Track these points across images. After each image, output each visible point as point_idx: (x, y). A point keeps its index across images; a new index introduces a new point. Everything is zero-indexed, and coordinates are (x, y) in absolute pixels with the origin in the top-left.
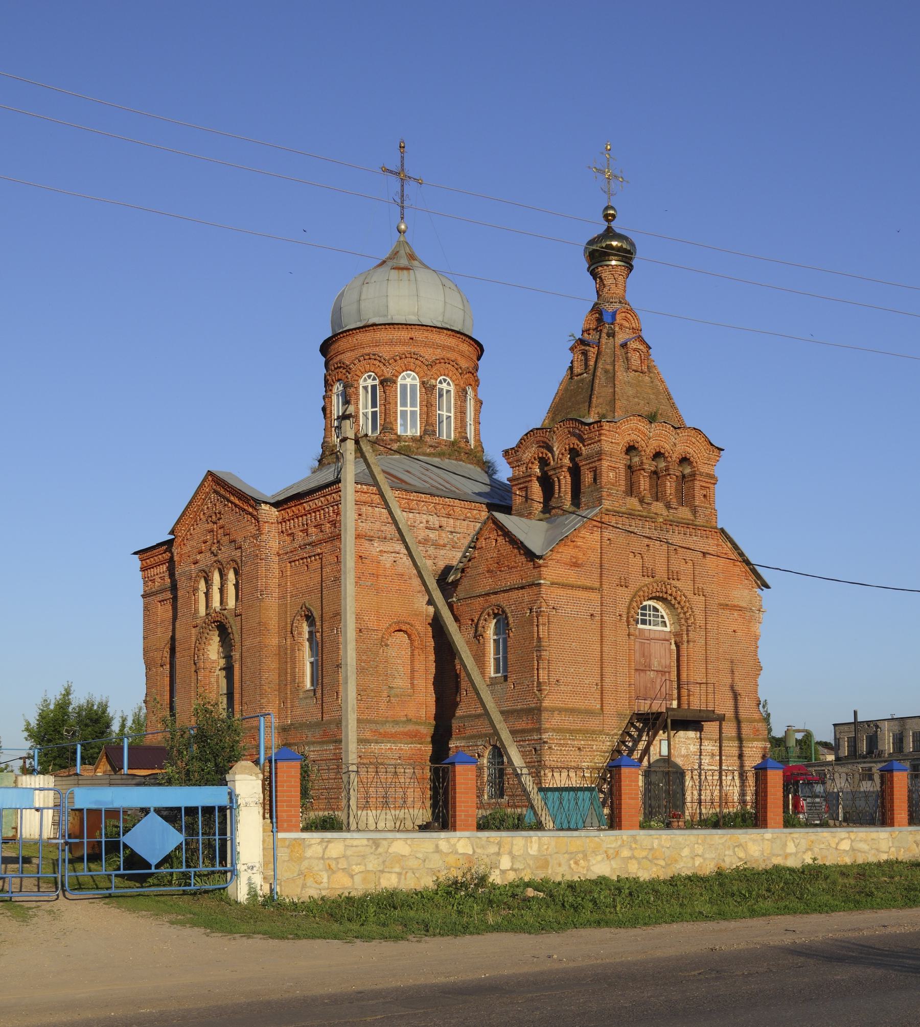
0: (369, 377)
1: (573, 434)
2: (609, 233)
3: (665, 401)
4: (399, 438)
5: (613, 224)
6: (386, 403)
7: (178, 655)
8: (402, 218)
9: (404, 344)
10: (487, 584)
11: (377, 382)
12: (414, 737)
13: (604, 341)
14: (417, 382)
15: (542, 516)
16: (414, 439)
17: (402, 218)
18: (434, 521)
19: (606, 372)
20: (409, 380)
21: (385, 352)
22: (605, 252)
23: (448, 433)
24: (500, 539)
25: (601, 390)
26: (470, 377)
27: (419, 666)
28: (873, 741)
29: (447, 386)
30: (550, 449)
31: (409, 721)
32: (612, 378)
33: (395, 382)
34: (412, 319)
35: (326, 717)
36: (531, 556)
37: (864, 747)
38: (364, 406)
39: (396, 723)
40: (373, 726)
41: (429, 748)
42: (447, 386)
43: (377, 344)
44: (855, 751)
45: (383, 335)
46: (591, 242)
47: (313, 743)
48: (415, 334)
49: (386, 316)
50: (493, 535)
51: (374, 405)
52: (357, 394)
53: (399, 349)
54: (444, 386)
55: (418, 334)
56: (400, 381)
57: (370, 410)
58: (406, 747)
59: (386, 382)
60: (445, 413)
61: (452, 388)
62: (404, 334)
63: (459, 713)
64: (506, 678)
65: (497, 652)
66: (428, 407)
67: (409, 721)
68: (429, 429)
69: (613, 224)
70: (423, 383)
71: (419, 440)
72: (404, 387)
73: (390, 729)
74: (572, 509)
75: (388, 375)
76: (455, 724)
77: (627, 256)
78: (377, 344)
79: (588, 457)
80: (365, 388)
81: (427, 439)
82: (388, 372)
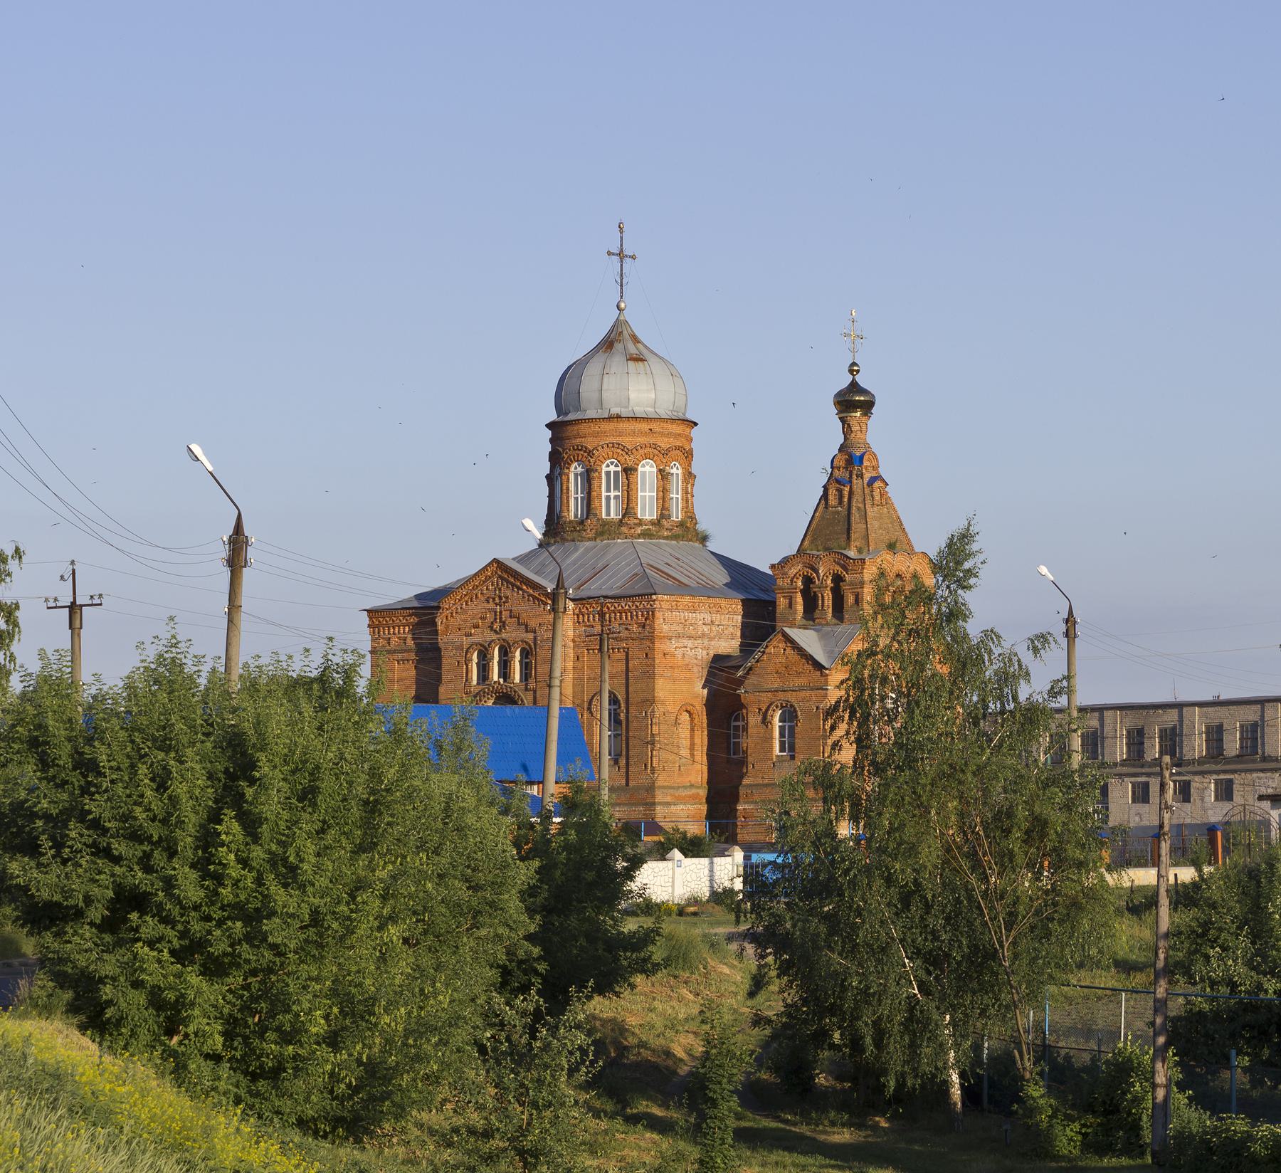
1: (838, 564)
2: (854, 387)
3: (898, 528)
4: (641, 523)
9: (645, 434)
10: (776, 683)
11: (619, 469)
12: (694, 798)
13: (854, 481)
14: (655, 470)
15: (804, 622)
16: (652, 523)
18: (708, 618)
19: (859, 509)
20: (647, 470)
21: (627, 442)
22: (853, 402)
23: (677, 515)
24: (789, 651)
25: (857, 527)
27: (697, 740)
28: (1172, 740)
30: (816, 571)
31: (692, 786)
32: (865, 516)
33: (636, 470)
34: (650, 411)
35: (631, 784)
36: (818, 666)
37: (1233, 745)
39: (685, 787)
40: (671, 791)
41: (704, 808)
43: (621, 434)
44: (1255, 747)
45: (623, 426)
46: (839, 394)
47: (619, 805)
48: (654, 425)
49: (626, 407)
50: (782, 645)
52: (600, 478)
53: (642, 440)
54: (674, 471)
55: (656, 426)
56: (640, 469)
58: (691, 807)
59: (629, 471)
61: (680, 472)
62: (645, 426)
63: (745, 781)
64: (793, 758)
65: (782, 735)
66: (664, 492)
67: (692, 786)
70: (660, 471)
71: (657, 523)
72: (644, 473)
73: (682, 793)
74: (835, 621)
75: (630, 464)
76: (742, 791)
78: (621, 434)
79: (851, 584)
81: (664, 522)
82: (630, 461)
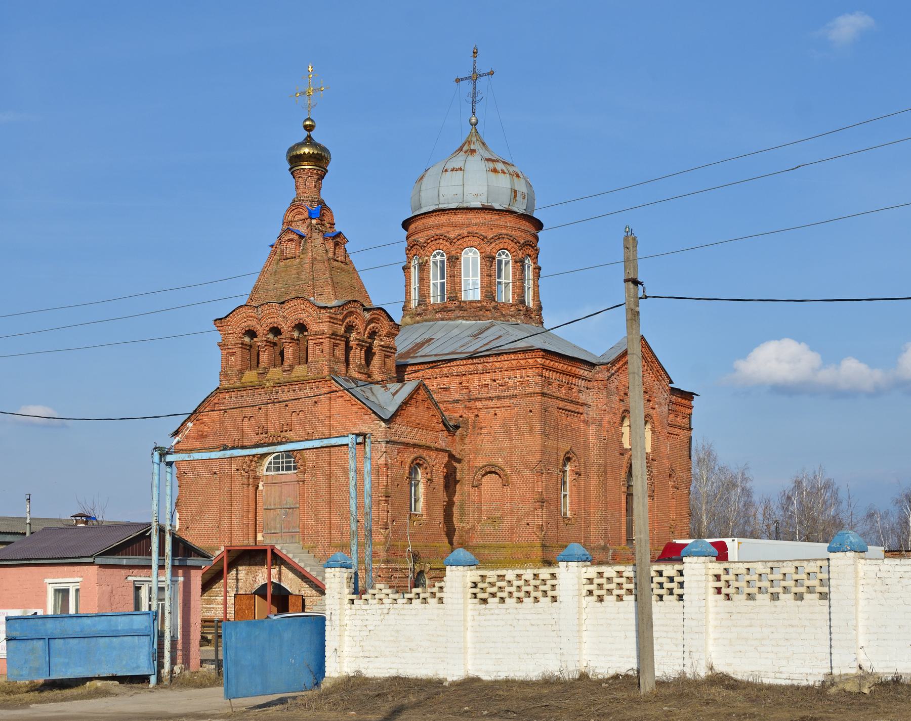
0: (438, 253)
2: (309, 141)
5: (312, 134)
6: (452, 276)
7: (132, 602)
8: (474, 113)
11: (445, 258)
17: (474, 113)
26: (530, 247)
29: (506, 258)
38: (435, 280)
42: (506, 258)
46: (292, 149)
51: (442, 278)
57: (439, 281)
59: (454, 260)
60: (503, 280)
68: (489, 295)
69: (312, 134)
75: (453, 253)
77: (295, 160)
80: (435, 263)
